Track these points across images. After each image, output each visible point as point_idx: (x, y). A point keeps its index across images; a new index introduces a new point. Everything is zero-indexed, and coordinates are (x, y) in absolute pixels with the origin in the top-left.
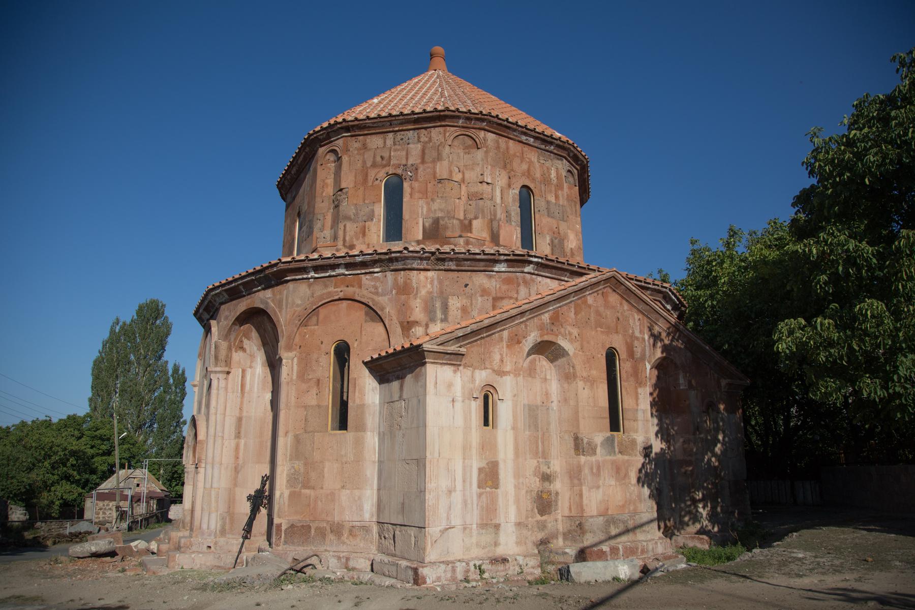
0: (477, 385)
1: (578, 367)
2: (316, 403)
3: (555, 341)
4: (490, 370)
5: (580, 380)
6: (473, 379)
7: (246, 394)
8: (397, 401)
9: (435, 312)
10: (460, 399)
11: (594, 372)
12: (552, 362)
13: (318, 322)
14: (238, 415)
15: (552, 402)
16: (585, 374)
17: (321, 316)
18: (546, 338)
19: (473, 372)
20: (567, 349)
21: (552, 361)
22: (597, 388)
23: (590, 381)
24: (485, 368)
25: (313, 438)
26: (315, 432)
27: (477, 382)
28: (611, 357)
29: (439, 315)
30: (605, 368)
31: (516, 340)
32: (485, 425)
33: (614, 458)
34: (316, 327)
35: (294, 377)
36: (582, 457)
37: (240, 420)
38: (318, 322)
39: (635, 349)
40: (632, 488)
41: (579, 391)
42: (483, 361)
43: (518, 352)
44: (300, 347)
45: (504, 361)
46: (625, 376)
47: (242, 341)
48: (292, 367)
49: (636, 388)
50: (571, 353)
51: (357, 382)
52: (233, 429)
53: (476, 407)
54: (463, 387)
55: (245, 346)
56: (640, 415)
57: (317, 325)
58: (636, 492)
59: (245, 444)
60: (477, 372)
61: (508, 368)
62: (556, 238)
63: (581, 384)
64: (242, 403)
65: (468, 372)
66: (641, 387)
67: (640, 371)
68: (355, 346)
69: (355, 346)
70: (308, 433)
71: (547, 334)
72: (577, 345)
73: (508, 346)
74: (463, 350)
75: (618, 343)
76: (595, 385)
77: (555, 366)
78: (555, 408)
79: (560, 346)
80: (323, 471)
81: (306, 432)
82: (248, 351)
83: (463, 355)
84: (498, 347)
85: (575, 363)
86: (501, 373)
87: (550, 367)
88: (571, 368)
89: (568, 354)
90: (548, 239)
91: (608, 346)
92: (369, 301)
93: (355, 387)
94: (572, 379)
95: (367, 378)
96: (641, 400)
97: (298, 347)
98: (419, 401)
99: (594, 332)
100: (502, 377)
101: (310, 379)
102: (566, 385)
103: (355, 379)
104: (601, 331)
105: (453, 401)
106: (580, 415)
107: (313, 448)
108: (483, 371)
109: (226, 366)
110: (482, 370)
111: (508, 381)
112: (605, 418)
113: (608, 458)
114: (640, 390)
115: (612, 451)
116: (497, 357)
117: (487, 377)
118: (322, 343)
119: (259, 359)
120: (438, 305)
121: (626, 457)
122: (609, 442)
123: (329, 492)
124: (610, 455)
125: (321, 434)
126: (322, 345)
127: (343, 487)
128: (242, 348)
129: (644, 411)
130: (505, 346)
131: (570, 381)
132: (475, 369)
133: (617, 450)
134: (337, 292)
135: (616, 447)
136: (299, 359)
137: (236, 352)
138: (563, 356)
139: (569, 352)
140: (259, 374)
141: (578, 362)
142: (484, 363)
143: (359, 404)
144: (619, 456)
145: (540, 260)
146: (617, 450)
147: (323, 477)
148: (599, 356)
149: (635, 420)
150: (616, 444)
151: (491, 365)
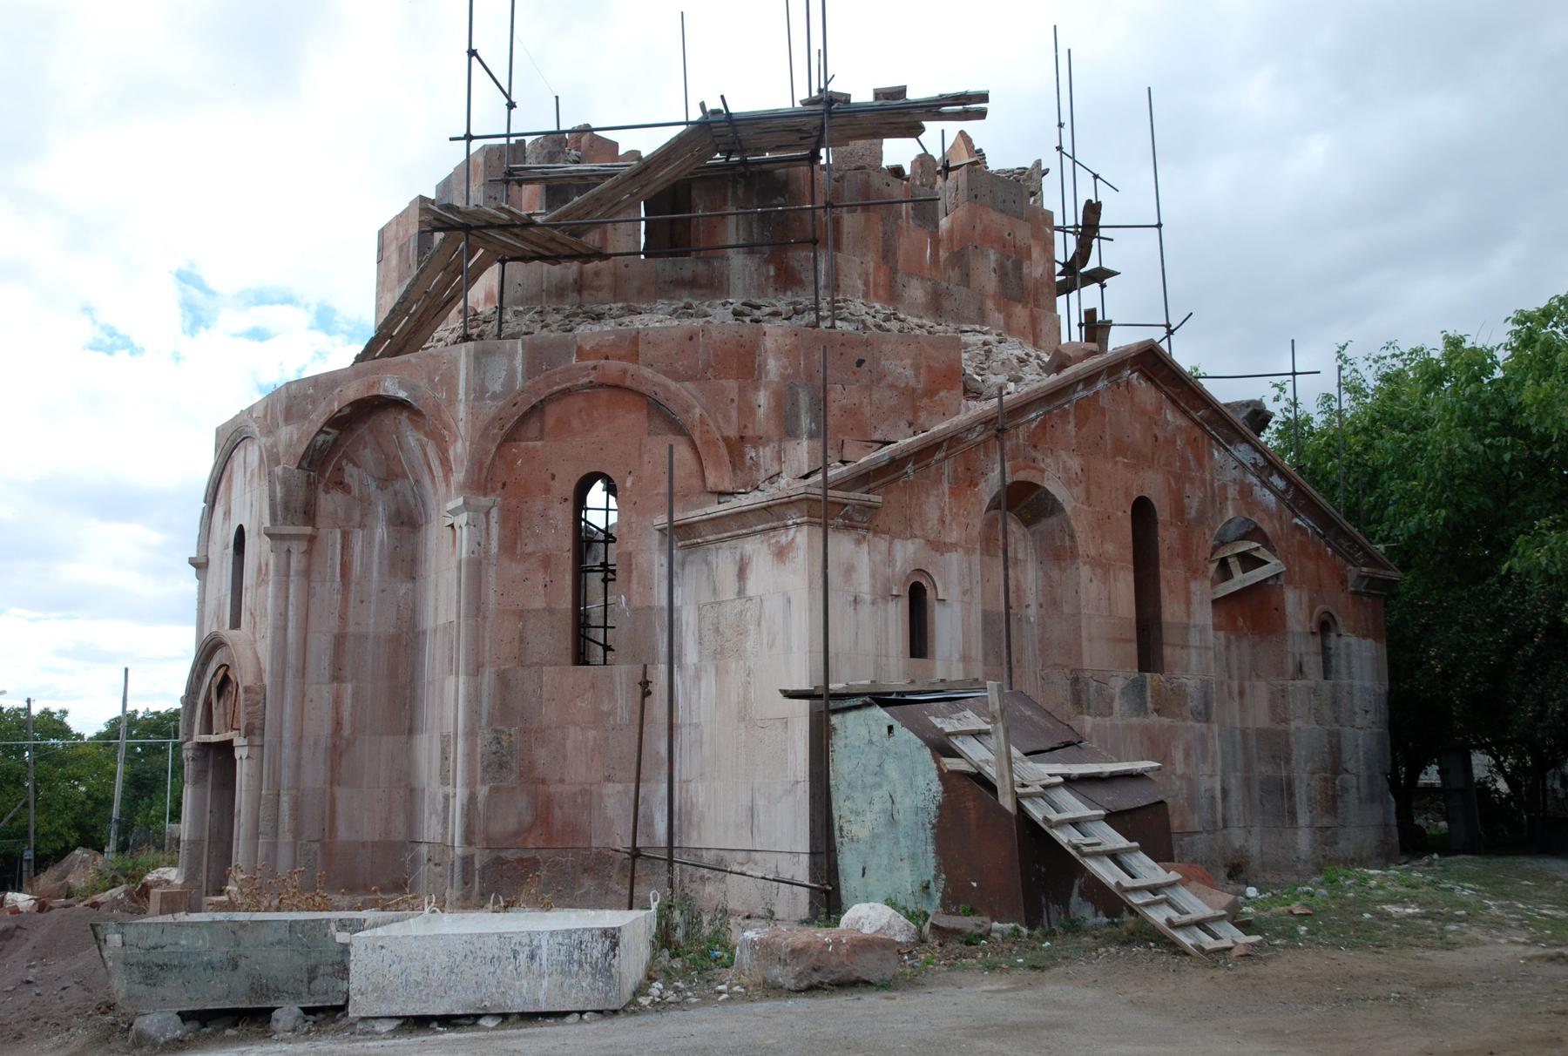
0: (897, 569)
1: (1081, 537)
2: (544, 605)
3: (1039, 483)
4: (922, 541)
5: (1085, 564)
6: (890, 560)
7: (353, 587)
8: (731, 600)
9: (798, 417)
10: (868, 597)
11: (1110, 547)
12: (1027, 526)
13: (542, 431)
14: (336, 631)
15: (1028, 606)
16: (1093, 553)
17: (550, 421)
18: (1022, 476)
19: (891, 544)
20: (1060, 499)
21: (1027, 523)
22: (1115, 580)
23: (1102, 565)
24: (913, 536)
25: (540, 678)
26: (542, 665)
27: (899, 564)
28: (1142, 510)
29: (805, 422)
30: (1130, 539)
31: (968, 480)
32: (913, 655)
33: (1146, 721)
34: (539, 443)
35: (494, 547)
36: (1087, 717)
37: (340, 640)
38: (542, 431)
39: (1186, 500)
40: (1178, 783)
41: (1082, 584)
42: (908, 522)
43: (972, 503)
44: (504, 485)
45: (947, 522)
46: (1166, 556)
47: (340, 469)
48: (488, 529)
49: (1187, 581)
50: (1068, 509)
51: (634, 561)
52: (326, 661)
53: (897, 615)
54: (873, 575)
55: (347, 480)
56: (1194, 638)
57: (541, 439)
58: (1185, 791)
59: (356, 695)
60: (898, 543)
61: (953, 536)
62: (1008, 258)
63: (1085, 571)
64: (345, 600)
65: (882, 544)
66: (1196, 579)
67: (1195, 547)
68: (628, 484)
69: (628, 484)
70: (529, 666)
71: (1026, 467)
72: (1079, 491)
73: (952, 492)
74: (876, 499)
75: (1153, 485)
76: (1112, 573)
77: (1033, 534)
78: (1032, 619)
79: (1047, 492)
80: (564, 746)
81: (522, 664)
82: (355, 491)
83: (877, 508)
84: (935, 492)
85: (1075, 527)
86: (939, 546)
87: (1024, 535)
88: (1067, 538)
89: (1062, 510)
90: (993, 257)
91: (1136, 495)
92: (656, 389)
93: (630, 572)
94: (1069, 561)
95: (657, 552)
96: (1195, 606)
97: (500, 485)
98: (789, 601)
99: (1110, 466)
100: (942, 554)
101: (530, 555)
102: (1055, 574)
103: (630, 554)
104: (1124, 463)
105: (855, 601)
106: (1084, 634)
107: (540, 697)
108: (909, 542)
109: (306, 524)
110: (907, 539)
111: (954, 558)
112: (1128, 641)
113: (1135, 720)
114: (1194, 586)
115: (1141, 709)
116: (933, 515)
117: (915, 553)
118: (553, 477)
119: (380, 509)
120: (804, 399)
121: (1166, 721)
122: (1137, 688)
123: (578, 788)
124: (1138, 716)
125: (558, 668)
126: (552, 483)
127: (608, 779)
128: (341, 485)
129: (1203, 630)
130: (947, 491)
131: (1063, 564)
132: (893, 538)
133: (1150, 705)
134: (585, 368)
135: (1149, 699)
136: (501, 510)
137: (327, 492)
138: (1052, 513)
139: (1065, 505)
140: (382, 542)
141: (1080, 527)
142: (911, 527)
143: (638, 605)
144: (1154, 719)
145: (755, 225)
146: (1150, 705)
147: (565, 757)
148: (1120, 514)
149: (1185, 647)
150: (1149, 693)
151: (923, 530)
